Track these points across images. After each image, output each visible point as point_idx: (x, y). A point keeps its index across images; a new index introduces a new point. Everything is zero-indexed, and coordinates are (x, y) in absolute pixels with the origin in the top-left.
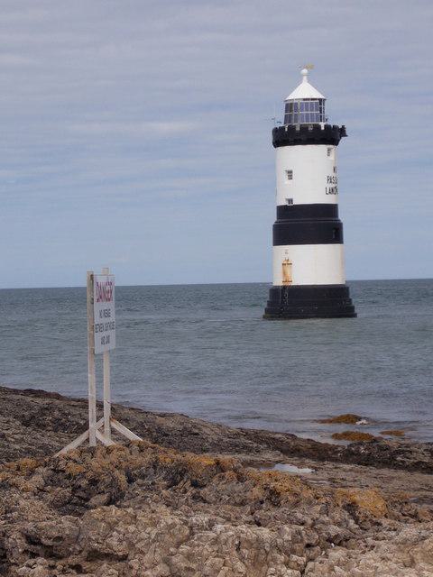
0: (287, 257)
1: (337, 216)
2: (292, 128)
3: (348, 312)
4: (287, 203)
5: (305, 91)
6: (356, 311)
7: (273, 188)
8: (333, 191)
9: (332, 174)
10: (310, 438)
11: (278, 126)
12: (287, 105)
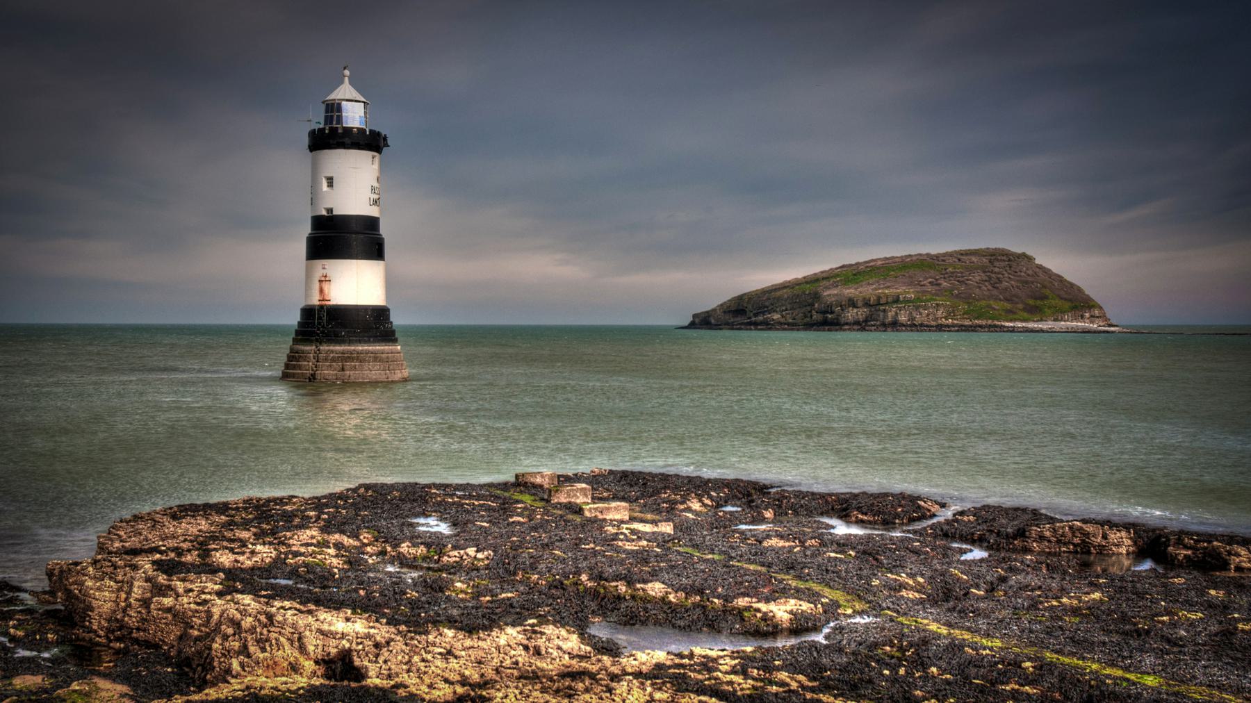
0: (325, 272)
1: (379, 231)
2: (334, 130)
3: (388, 336)
4: (324, 213)
6: (397, 336)
7: (314, 200)
8: (376, 202)
10: (627, 466)
11: (316, 127)
12: (327, 105)
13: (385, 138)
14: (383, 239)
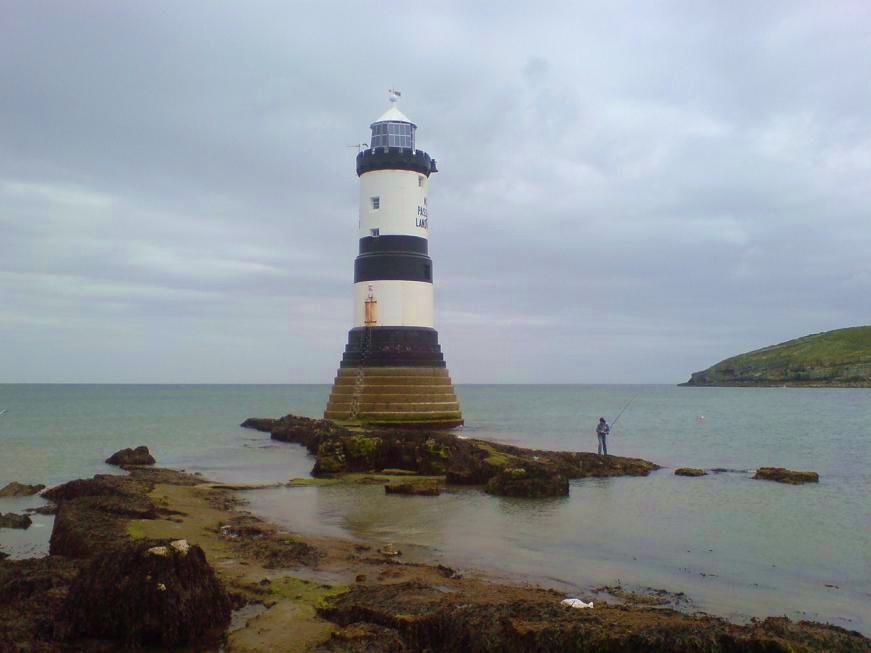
5: (394, 114)
8: (423, 224)
9: (422, 205)
11: (364, 149)
13: (433, 162)
14: (430, 261)
